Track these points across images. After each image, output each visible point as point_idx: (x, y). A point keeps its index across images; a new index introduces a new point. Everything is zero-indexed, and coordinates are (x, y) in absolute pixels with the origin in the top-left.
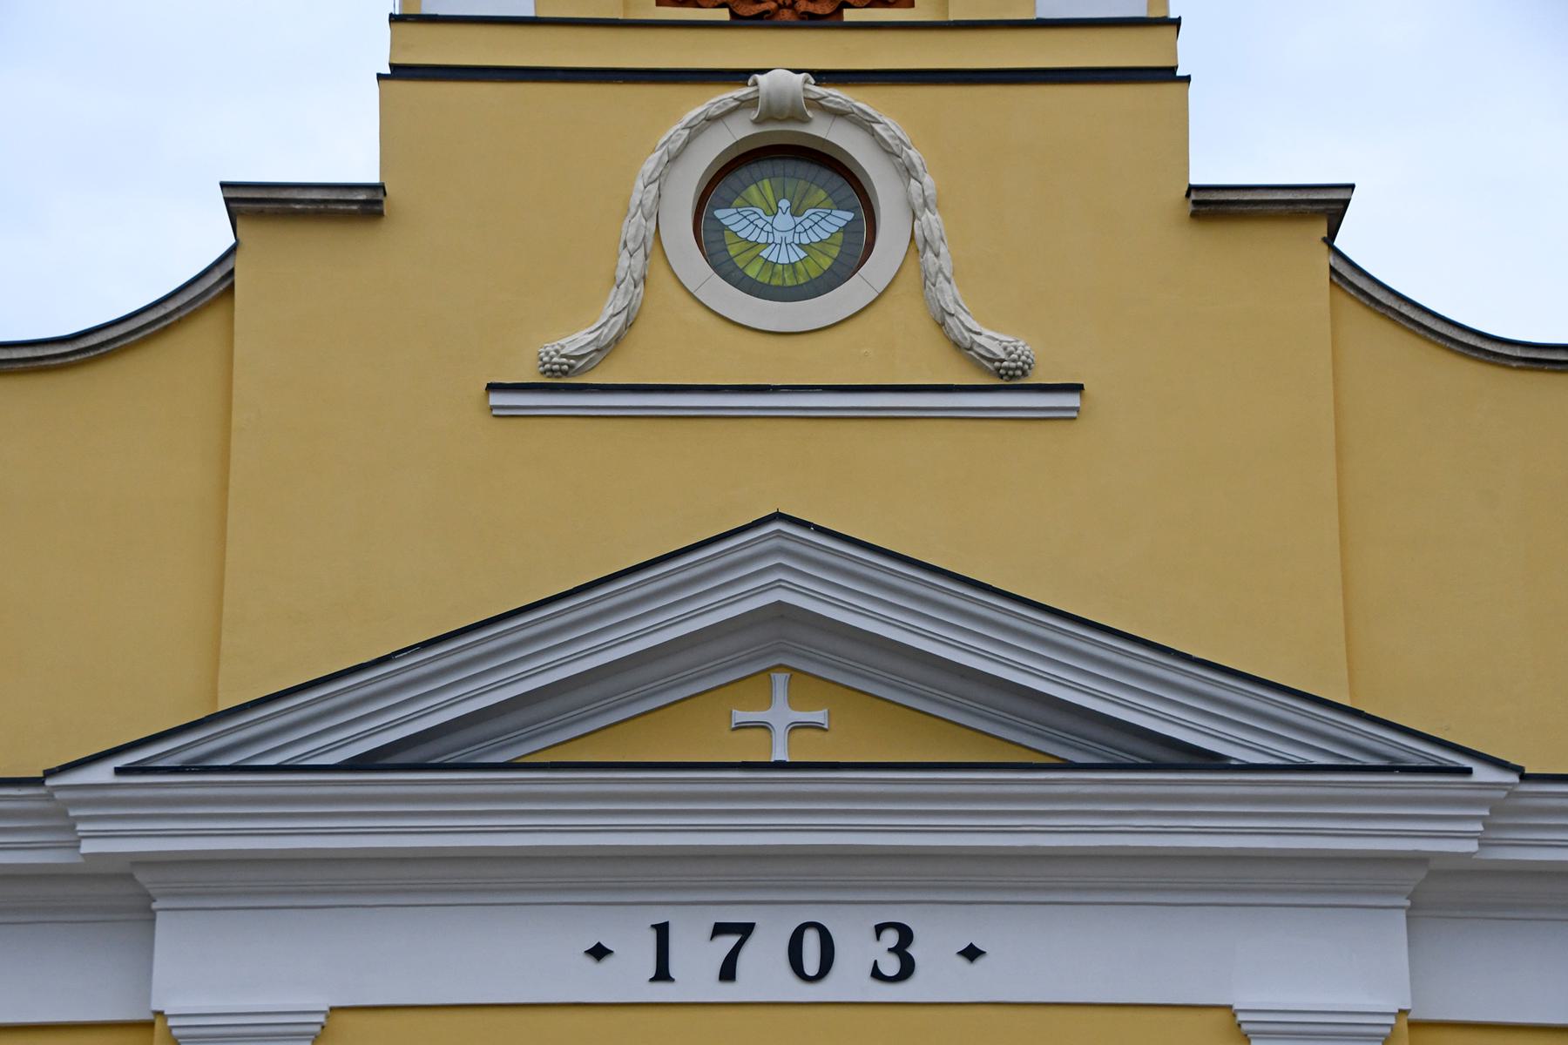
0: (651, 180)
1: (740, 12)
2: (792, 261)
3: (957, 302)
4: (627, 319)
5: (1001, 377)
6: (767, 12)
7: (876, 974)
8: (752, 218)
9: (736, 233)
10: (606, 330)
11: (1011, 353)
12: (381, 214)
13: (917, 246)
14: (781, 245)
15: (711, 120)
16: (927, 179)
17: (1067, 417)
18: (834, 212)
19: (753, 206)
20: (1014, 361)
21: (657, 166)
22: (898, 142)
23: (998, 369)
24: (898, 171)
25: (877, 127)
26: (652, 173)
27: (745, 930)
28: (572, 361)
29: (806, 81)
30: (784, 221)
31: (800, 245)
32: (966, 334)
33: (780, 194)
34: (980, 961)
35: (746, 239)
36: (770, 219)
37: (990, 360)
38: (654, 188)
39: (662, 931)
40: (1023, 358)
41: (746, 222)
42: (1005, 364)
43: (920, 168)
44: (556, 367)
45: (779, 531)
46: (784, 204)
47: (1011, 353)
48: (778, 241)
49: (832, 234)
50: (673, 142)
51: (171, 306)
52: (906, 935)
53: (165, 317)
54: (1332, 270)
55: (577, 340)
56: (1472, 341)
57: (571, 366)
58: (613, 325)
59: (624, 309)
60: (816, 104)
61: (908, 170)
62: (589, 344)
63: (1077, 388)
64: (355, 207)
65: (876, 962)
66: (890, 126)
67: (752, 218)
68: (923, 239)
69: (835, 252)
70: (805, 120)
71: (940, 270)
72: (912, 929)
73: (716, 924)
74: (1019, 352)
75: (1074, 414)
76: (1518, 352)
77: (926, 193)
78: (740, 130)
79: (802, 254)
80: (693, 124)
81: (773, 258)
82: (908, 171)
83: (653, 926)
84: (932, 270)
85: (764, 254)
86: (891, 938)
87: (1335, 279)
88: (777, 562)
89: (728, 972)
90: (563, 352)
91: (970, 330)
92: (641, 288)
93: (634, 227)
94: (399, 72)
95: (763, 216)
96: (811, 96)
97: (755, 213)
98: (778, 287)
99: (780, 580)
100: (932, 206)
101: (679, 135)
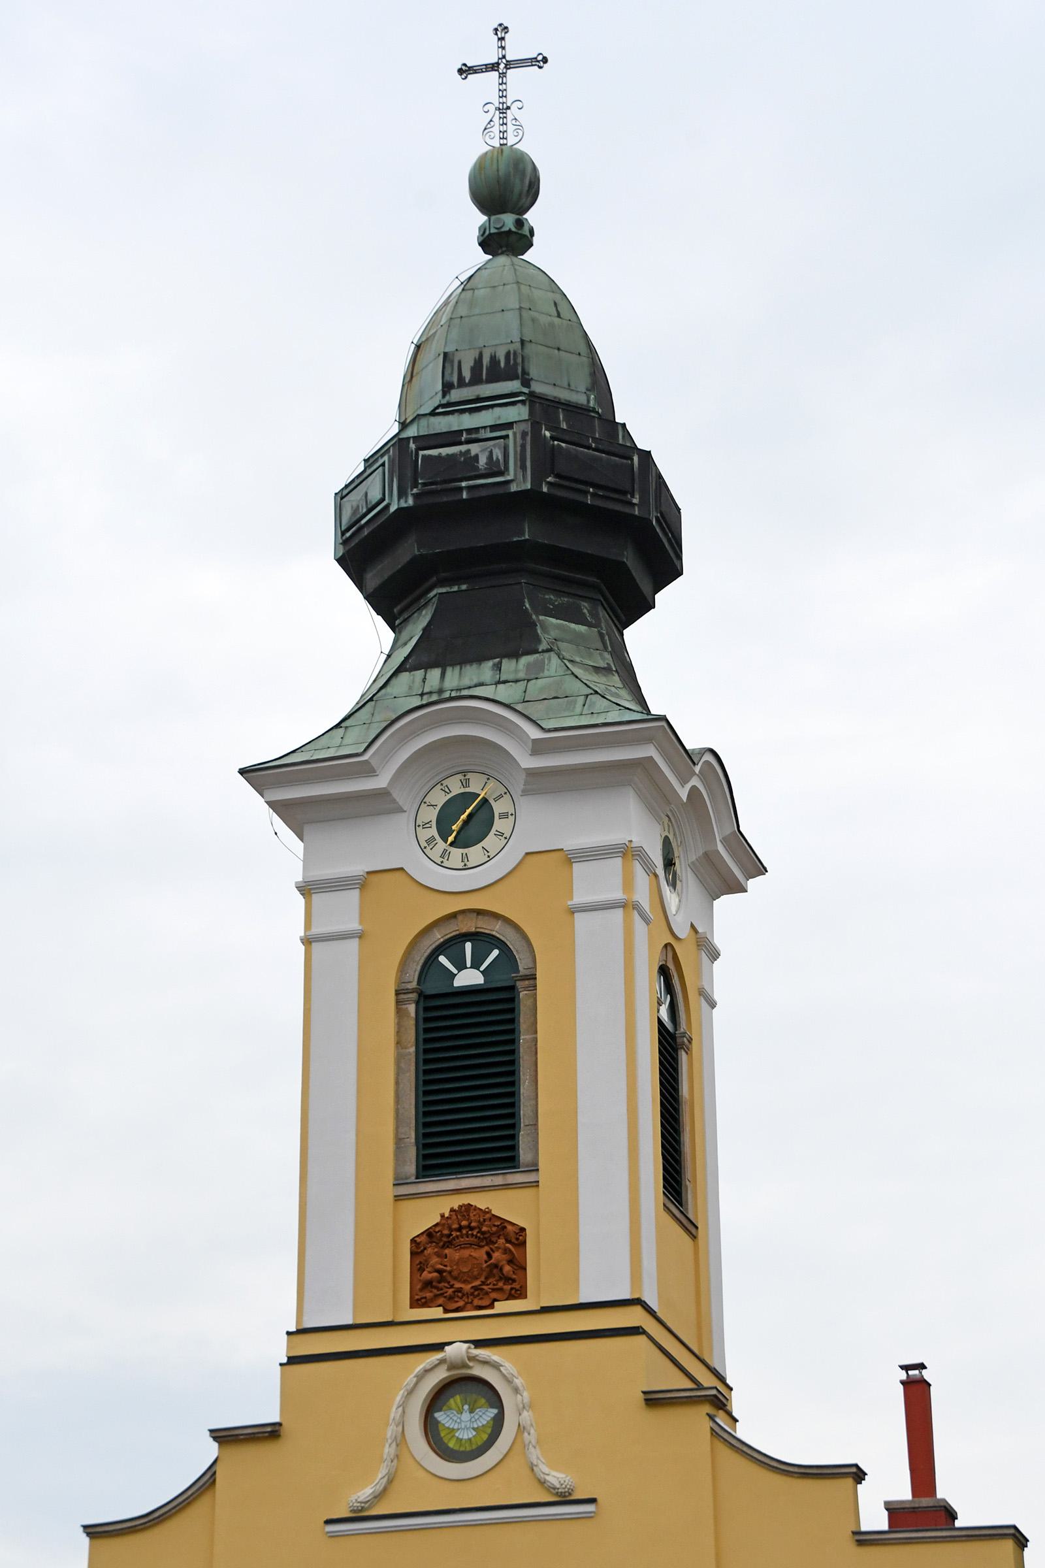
1: (448, 1308)
3: (538, 1458)
4: (388, 1479)
5: (560, 1496)
6: (459, 1307)
8: (451, 1416)
10: (378, 1487)
11: (562, 1485)
12: (279, 1436)
13: (521, 1429)
15: (427, 1371)
16: (525, 1394)
17: (588, 1517)
20: (564, 1488)
21: (402, 1398)
22: (511, 1375)
23: (557, 1493)
25: (502, 1368)
28: (363, 1505)
29: (469, 1348)
30: (466, 1416)
32: (542, 1476)
33: (465, 1402)
36: (459, 1416)
38: (401, 1409)
40: (568, 1486)
41: (448, 1418)
43: (521, 1388)
44: (355, 1508)
46: (466, 1407)
48: (463, 1427)
51: (190, 1493)
53: (187, 1499)
54: (712, 1429)
55: (366, 1493)
56: (775, 1464)
57: (362, 1507)
58: (381, 1484)
60: (473, 1358)
63: (592, 1501)
64: (267, 1434)
66: (508, 1367)
67: (451, 1416)
69: (489, 1431)
70: (470, 1367)
71: (530, 1442)
74: (566, 1484)
75: (592, 1515)
76: (796, 1470)
77: (524, 1402)
78: (442, 1374)
79: (474, 1433)
81: (461, 1437)
82: (516, 1390)
84: (527, 1442)
85: (457, 1434)
90: (359, 1500)
91: (544, 1474)
92: (395, 1461)
93: (391, 1431)
94: (292, 1360)
95: (457, 1414)
96: (471, 1355)
98: (463, 1452)
100: (527, 1408)
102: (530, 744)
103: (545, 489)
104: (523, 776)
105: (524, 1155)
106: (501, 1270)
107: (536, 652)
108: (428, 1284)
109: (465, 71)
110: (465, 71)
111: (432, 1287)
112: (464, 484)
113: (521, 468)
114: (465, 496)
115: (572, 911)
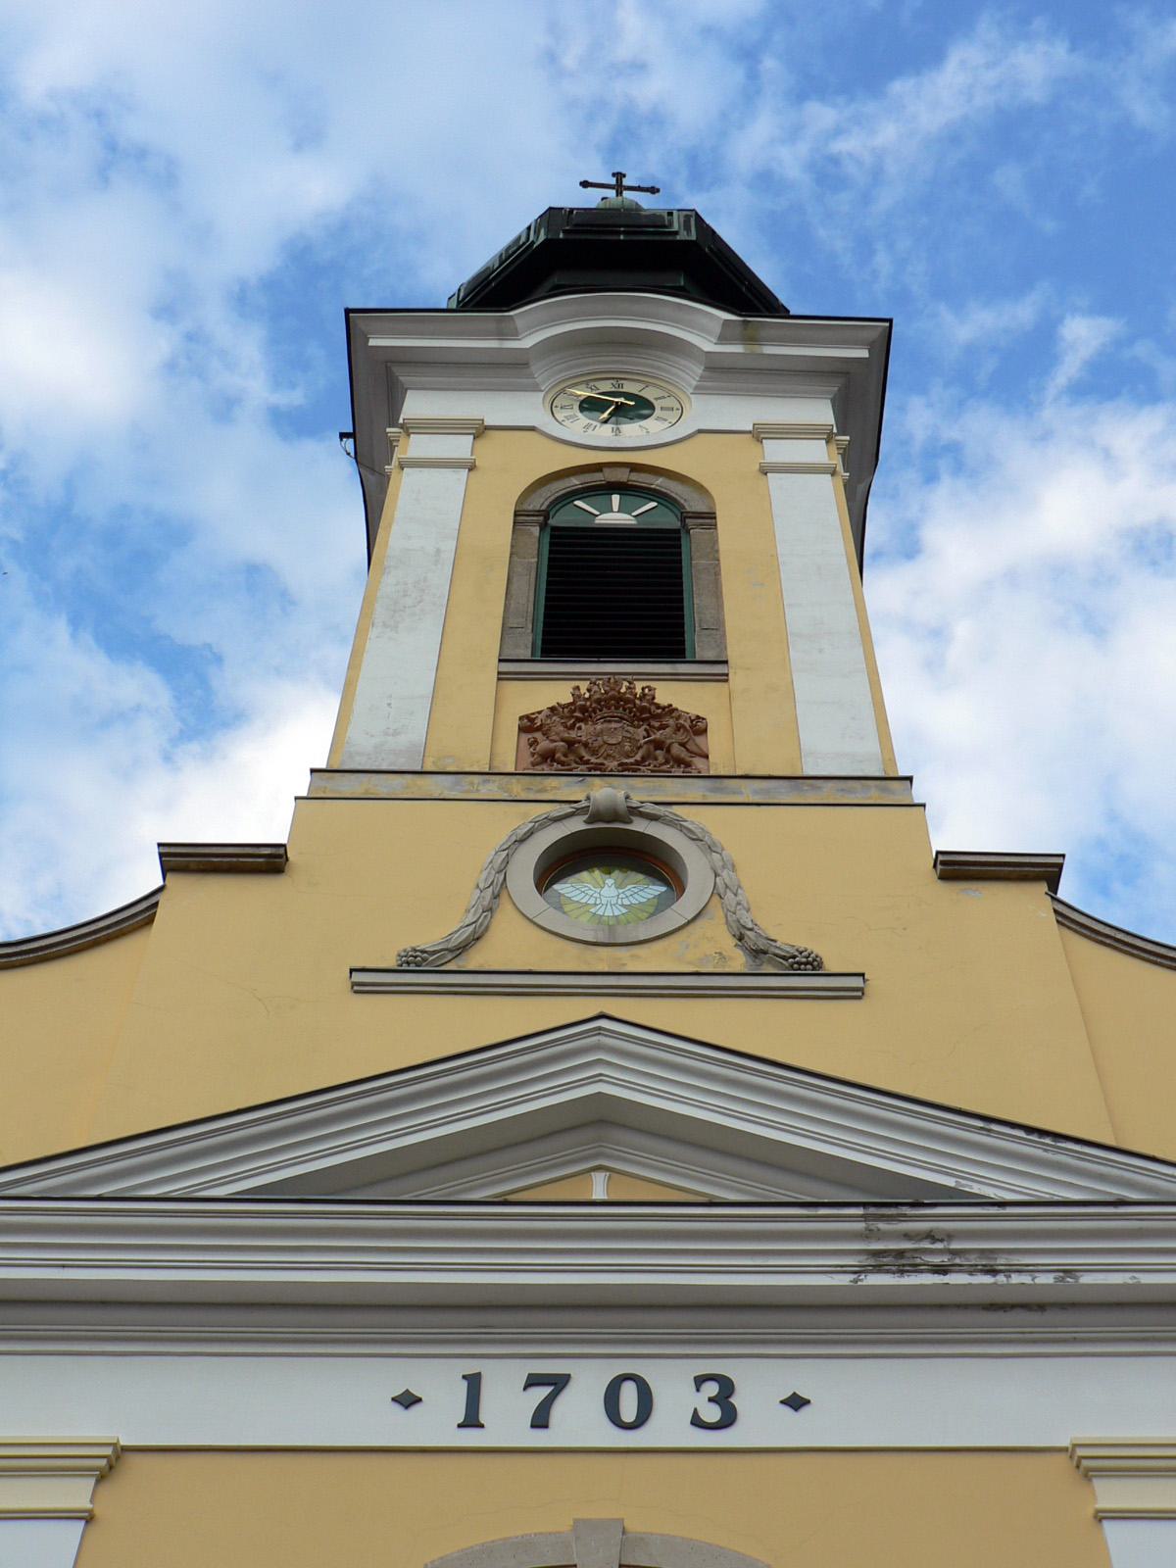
2: (616, 914)
4: (474, 932)
7: (697, 1422)
11: (801, 953)
24: (702, 850)
26: (503, 844)
27: (559, 1383)
31: (623, 905)
34: (805, 1410)
39: (474, 1382)
45: (600, 1028)
48: (604, 901)
52: (727, 1387)
59: (473, 923)
61: (710, 847)
65: (696, 1410)
72: (731, 1377)
79: (624, 911)
80: (537, 819)
81: (600, 913)
83: (464, 1377)
86: (712, 1389)
87: (1060, 919)
88: (597, 1058)
89: (541, 1420)
99: (601, 1075)
102: (718, 329)
103: (707, 250)
104: (699, 370)
105: (701, 646)
106: (668, 751)
107: (630, 514)
108: (548, 757)
109: (585, 184)
110: (585, 184)
111: (553, 760)
112: (622, 229)
113: (685, 229)
114: (622, 237)
115: (765, 471)
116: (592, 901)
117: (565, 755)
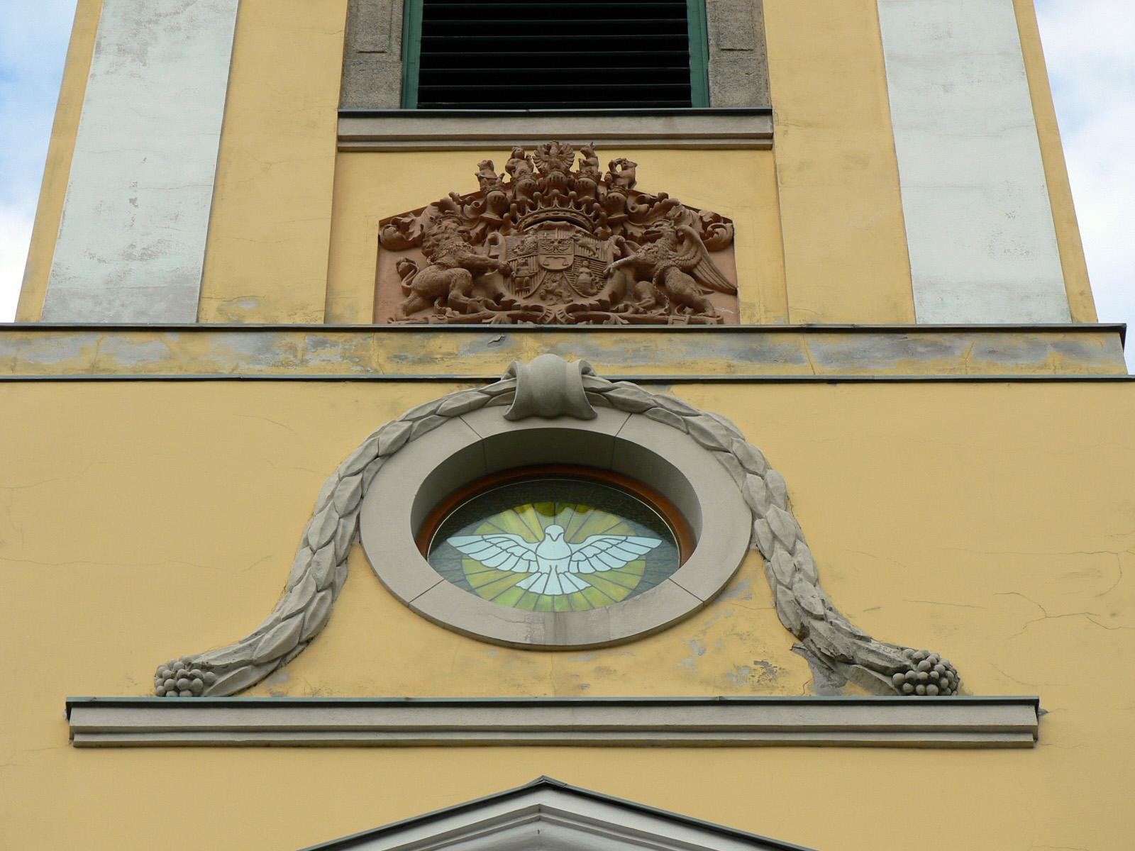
0: (350, 472)
9: (480, 561)
14: (549, 574)
18: (630, 539)
19: (507, 533)
35: (496, 568)
37: (885, 671)
42: (910, 674)
47: (917, 661)
49: (628, 562)
50: (386, 433)
62: (235, 652)
68: (770, 536)
70: (592, 417)
73: (380, 221)
79: (582, 584)
81: (537, 588)
97: (510, 540)
101: (396, 426)
108: (435, 296)
116: (522, 567)
117: (468, 294)
